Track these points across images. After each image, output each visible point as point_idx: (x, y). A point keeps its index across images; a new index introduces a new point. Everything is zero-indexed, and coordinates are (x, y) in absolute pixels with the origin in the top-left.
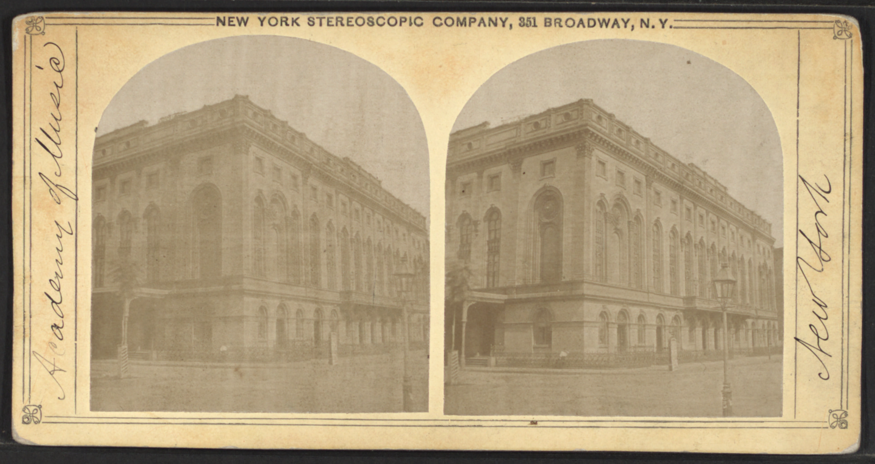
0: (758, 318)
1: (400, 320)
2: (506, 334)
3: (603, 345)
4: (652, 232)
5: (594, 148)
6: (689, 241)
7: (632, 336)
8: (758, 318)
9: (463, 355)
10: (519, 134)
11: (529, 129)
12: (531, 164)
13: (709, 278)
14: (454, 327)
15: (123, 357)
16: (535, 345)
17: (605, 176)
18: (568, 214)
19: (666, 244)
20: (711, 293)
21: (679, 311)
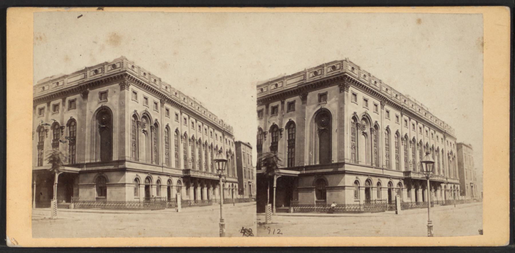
0: (448, 183)
2: (299, 194)
3: (188, 196)
5: (130, 84)
6: (186, 137)
7: (153, 191)
8: (448, 183)
9: (274, 207)
10: (305, 78)
11: (311, 75)
12: (94, 94)
13: (418, 160)
15: (268, 213)
16: (317, 200)
17: (137, 100)
19: (393, 140)
21: (171, 176)
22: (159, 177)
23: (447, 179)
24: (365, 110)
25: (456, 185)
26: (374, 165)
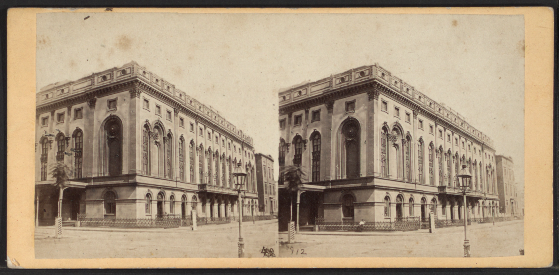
0: (486, 199)
1: (477, 204)
2: (325, 211)
3: (204, 213)
4: (178, 143)
5: (141, 91)
6: (201, 149)
7: (166, 208)
8: (486, 199)
9: (298, 225)
10: (331, 85)
11: (338, 82)
12: (102, 102)
13: (454, 174)
14: (291, 207)
17: (148, 108)
18: (363, 136)
19: (427, 152)
20: (456, 184)
22: (172, 193)
23: (485, 194)
24: (396, 119)
25: (495, 202)
26: (406, 180)
